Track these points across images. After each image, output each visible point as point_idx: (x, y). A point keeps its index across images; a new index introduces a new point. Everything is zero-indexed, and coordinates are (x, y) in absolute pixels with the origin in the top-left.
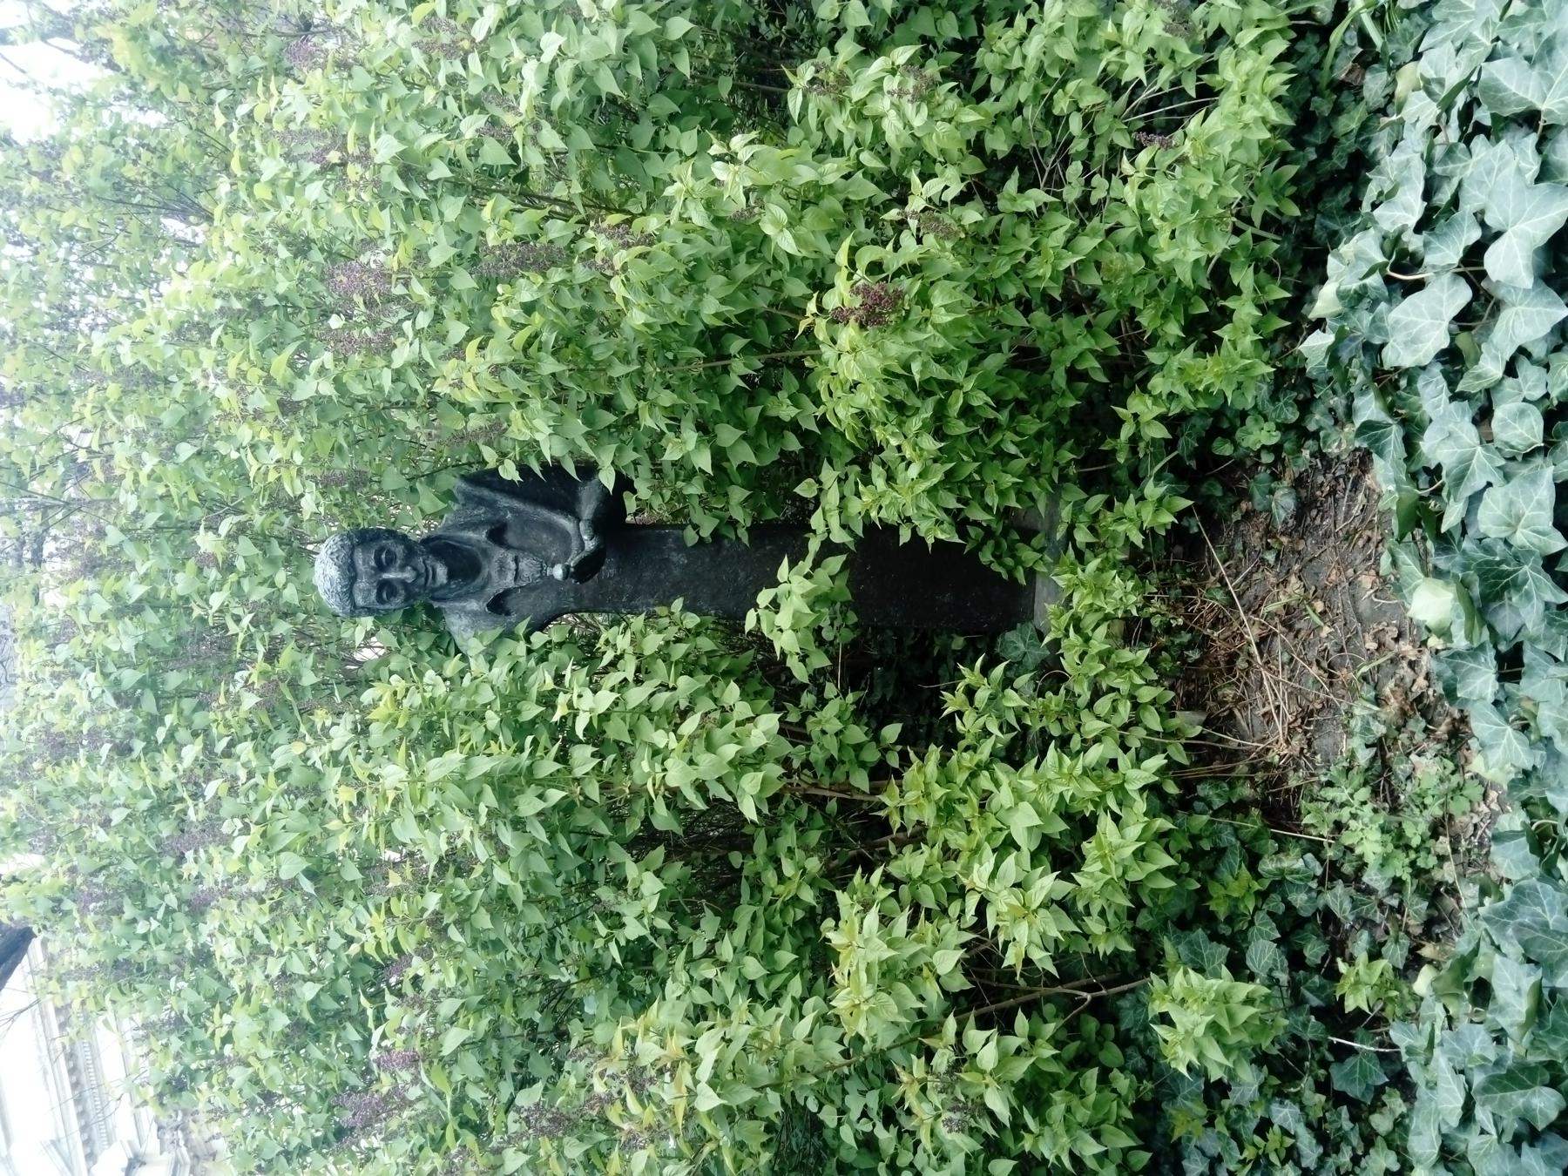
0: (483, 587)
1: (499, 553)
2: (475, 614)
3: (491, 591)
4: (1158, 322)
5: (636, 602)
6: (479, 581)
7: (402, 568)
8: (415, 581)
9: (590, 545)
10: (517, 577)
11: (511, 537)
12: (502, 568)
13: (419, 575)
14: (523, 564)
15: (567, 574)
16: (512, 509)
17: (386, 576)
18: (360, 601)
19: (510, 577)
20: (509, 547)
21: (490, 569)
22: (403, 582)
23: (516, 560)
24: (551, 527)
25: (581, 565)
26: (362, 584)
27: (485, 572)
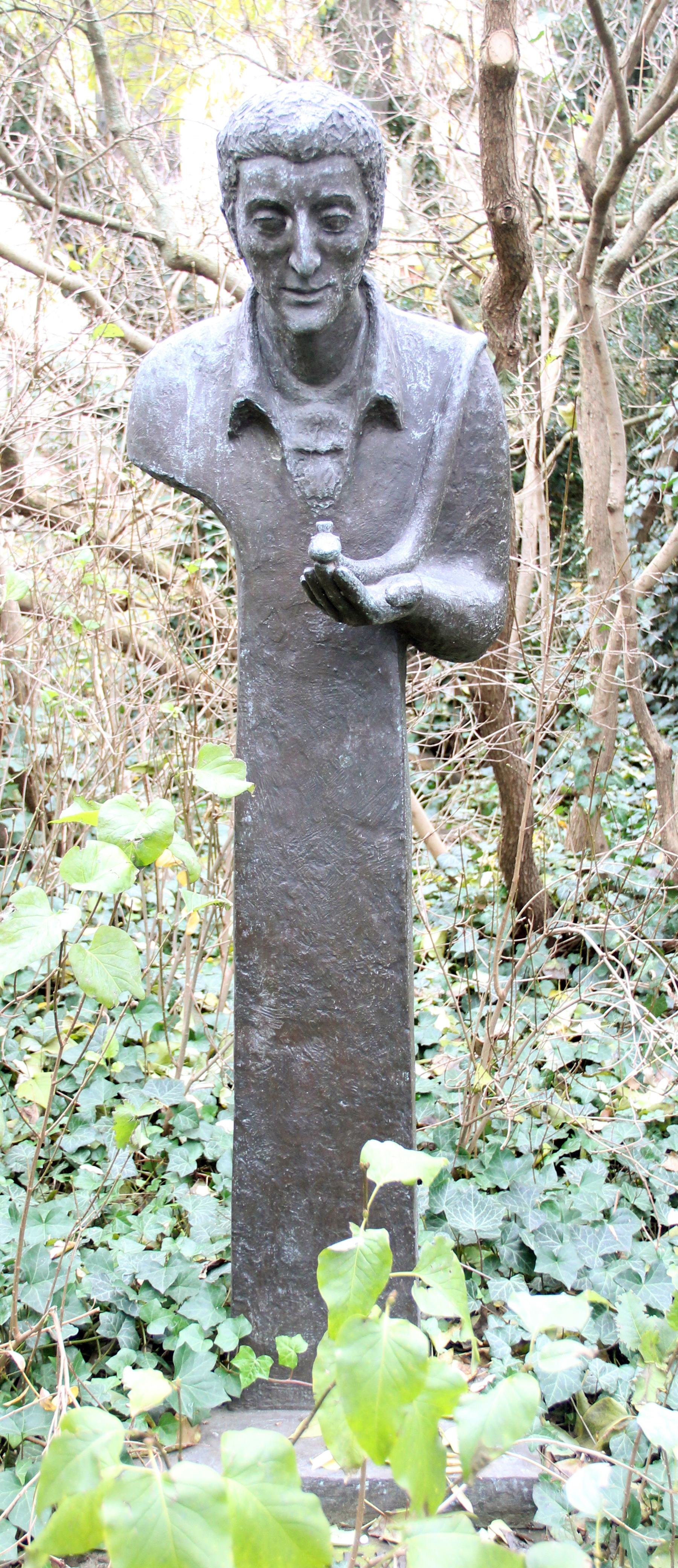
0: (280, 389)
1: (348, 418)
2: (228, 376)
3: (275, 408)
4: (472, 983)
5: (263, 675)
6: (293, 383)
7: (320, 248)
8: (539, 996)
9: (374, 596)
10: (303, 453)
11: (378, 438)
12: (319, 424)
13: (304, 278)
14: (329, 465)
15: (323, 560)
16: (431, 439)
17: (302, 217)
18: (251, 169)
19: (307, 440)
20: (358, 437)
21: (318, 403)
22: (289, 249)
23: (336, 451)
24: (400, 512)
25: (338, 583)
26: (287, 174)
27: (308, 392)
